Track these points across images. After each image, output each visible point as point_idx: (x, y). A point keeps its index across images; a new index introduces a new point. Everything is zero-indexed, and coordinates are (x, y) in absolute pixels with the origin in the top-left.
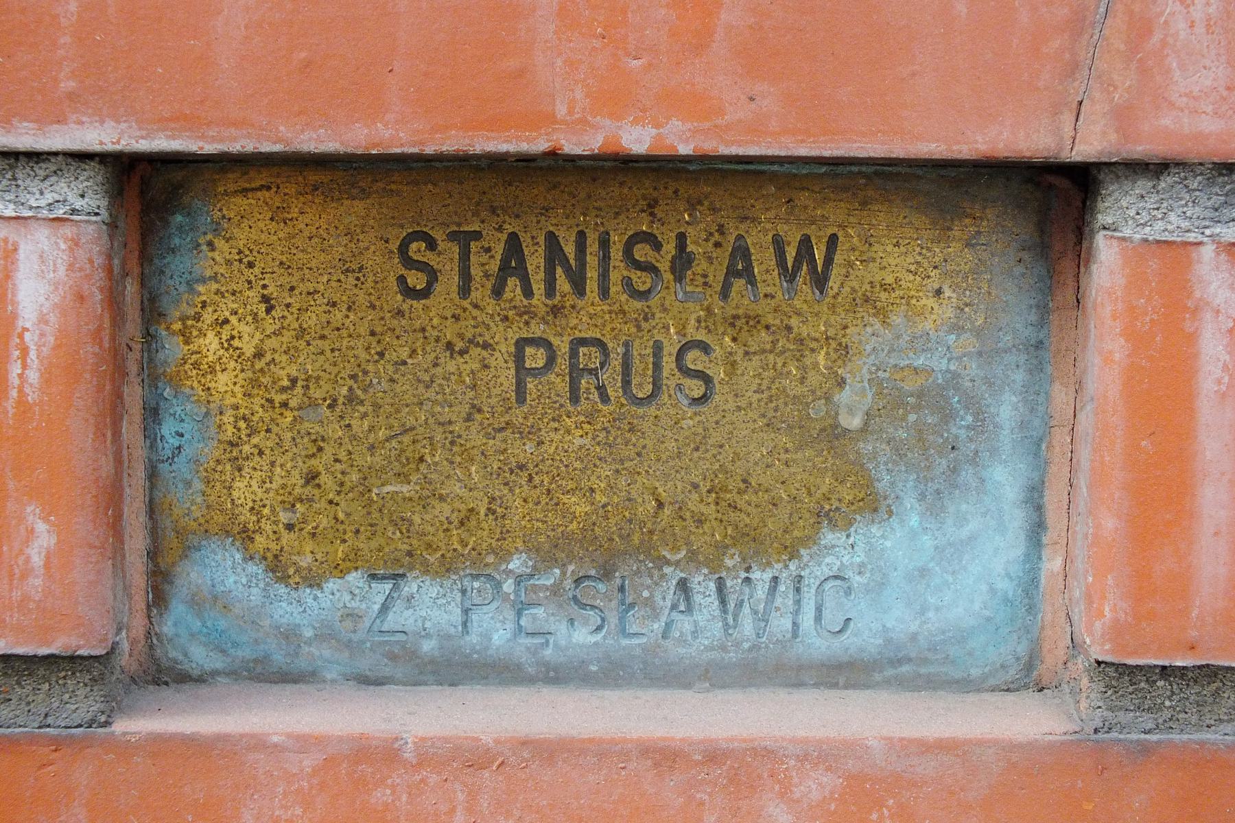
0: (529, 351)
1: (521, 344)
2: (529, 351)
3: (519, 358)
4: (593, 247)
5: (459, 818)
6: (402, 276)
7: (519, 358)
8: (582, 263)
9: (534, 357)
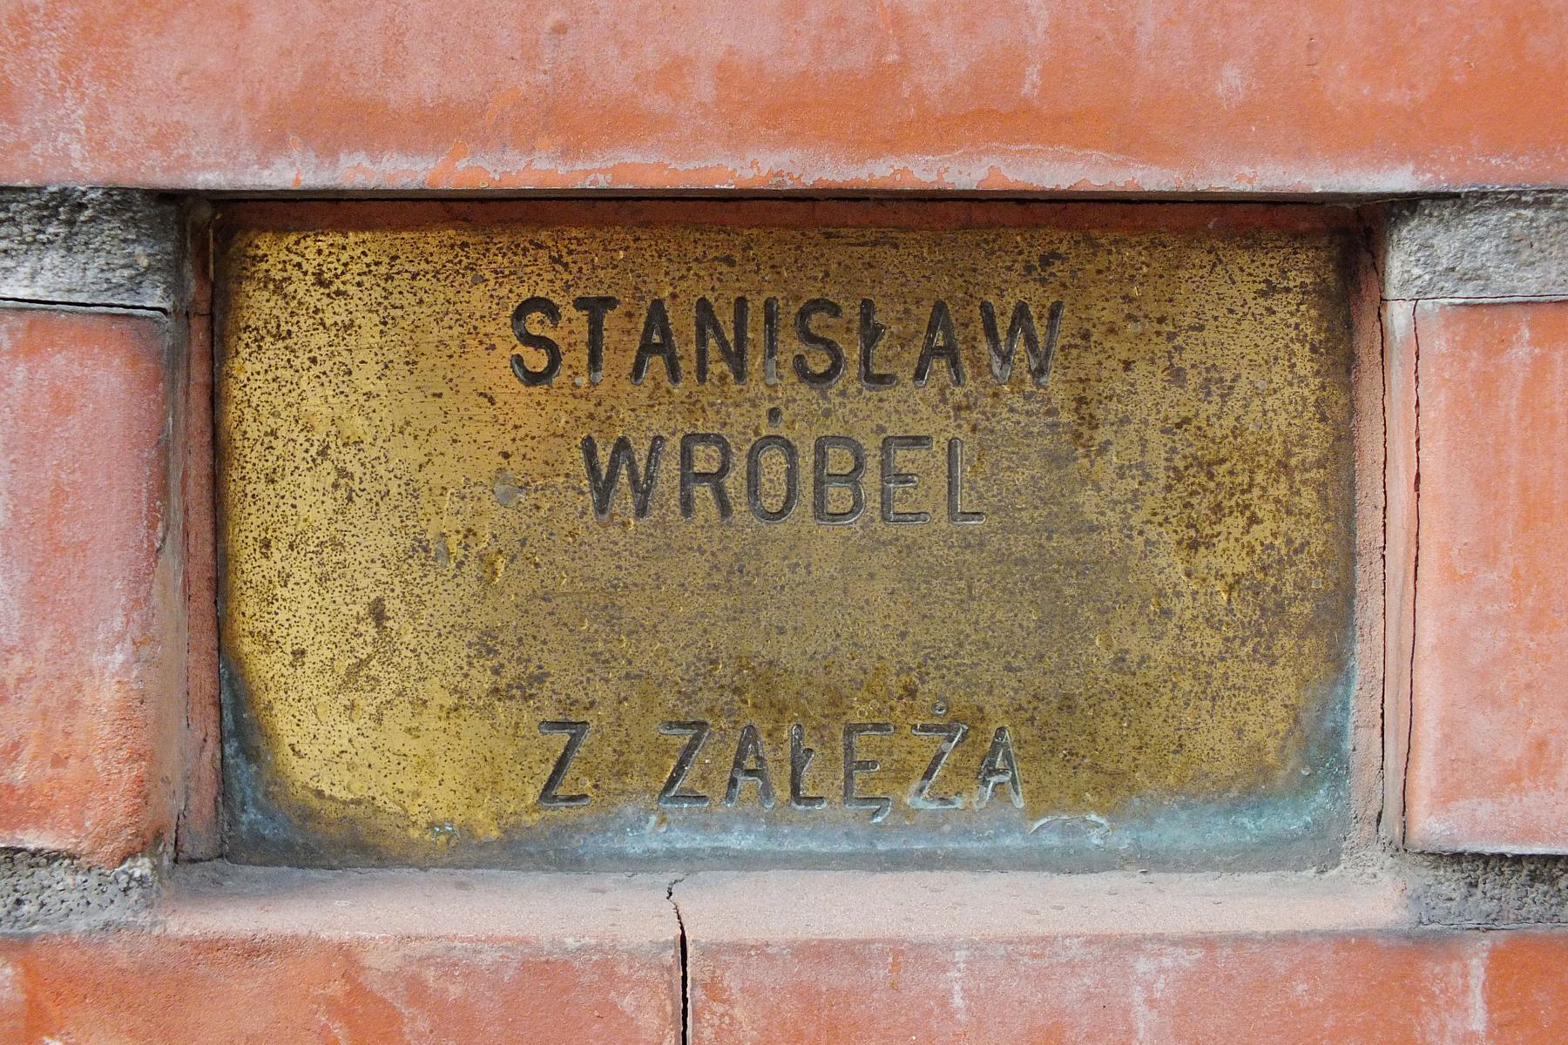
0: (699, 450)
1: (689, 440)
2: (699, 450)
3: (686, 457)
4: (756, 318)
5: (1, 215)
6: (799, 357)
7: (686, 457)
8: (740, 338)
9: (709, 458)
